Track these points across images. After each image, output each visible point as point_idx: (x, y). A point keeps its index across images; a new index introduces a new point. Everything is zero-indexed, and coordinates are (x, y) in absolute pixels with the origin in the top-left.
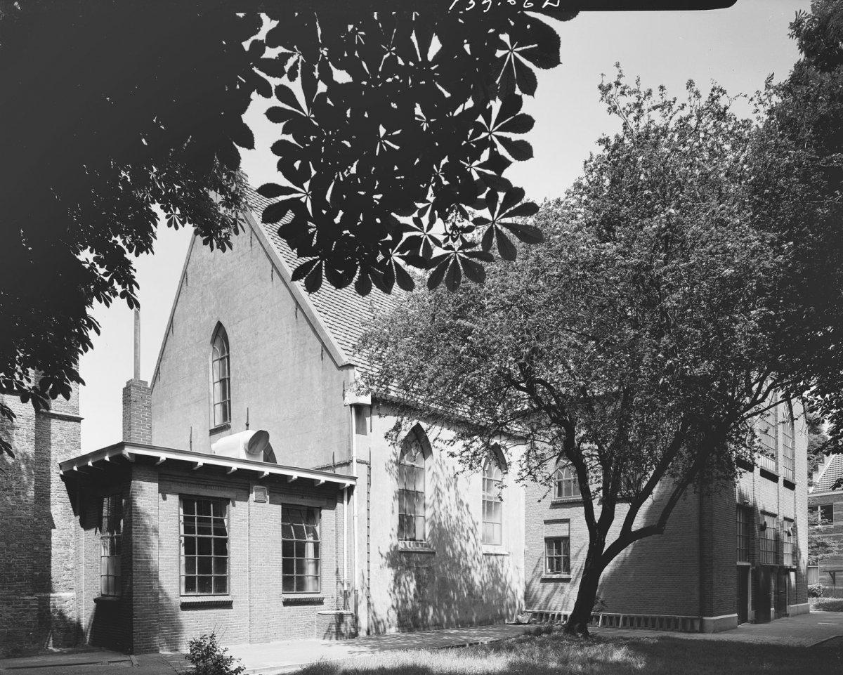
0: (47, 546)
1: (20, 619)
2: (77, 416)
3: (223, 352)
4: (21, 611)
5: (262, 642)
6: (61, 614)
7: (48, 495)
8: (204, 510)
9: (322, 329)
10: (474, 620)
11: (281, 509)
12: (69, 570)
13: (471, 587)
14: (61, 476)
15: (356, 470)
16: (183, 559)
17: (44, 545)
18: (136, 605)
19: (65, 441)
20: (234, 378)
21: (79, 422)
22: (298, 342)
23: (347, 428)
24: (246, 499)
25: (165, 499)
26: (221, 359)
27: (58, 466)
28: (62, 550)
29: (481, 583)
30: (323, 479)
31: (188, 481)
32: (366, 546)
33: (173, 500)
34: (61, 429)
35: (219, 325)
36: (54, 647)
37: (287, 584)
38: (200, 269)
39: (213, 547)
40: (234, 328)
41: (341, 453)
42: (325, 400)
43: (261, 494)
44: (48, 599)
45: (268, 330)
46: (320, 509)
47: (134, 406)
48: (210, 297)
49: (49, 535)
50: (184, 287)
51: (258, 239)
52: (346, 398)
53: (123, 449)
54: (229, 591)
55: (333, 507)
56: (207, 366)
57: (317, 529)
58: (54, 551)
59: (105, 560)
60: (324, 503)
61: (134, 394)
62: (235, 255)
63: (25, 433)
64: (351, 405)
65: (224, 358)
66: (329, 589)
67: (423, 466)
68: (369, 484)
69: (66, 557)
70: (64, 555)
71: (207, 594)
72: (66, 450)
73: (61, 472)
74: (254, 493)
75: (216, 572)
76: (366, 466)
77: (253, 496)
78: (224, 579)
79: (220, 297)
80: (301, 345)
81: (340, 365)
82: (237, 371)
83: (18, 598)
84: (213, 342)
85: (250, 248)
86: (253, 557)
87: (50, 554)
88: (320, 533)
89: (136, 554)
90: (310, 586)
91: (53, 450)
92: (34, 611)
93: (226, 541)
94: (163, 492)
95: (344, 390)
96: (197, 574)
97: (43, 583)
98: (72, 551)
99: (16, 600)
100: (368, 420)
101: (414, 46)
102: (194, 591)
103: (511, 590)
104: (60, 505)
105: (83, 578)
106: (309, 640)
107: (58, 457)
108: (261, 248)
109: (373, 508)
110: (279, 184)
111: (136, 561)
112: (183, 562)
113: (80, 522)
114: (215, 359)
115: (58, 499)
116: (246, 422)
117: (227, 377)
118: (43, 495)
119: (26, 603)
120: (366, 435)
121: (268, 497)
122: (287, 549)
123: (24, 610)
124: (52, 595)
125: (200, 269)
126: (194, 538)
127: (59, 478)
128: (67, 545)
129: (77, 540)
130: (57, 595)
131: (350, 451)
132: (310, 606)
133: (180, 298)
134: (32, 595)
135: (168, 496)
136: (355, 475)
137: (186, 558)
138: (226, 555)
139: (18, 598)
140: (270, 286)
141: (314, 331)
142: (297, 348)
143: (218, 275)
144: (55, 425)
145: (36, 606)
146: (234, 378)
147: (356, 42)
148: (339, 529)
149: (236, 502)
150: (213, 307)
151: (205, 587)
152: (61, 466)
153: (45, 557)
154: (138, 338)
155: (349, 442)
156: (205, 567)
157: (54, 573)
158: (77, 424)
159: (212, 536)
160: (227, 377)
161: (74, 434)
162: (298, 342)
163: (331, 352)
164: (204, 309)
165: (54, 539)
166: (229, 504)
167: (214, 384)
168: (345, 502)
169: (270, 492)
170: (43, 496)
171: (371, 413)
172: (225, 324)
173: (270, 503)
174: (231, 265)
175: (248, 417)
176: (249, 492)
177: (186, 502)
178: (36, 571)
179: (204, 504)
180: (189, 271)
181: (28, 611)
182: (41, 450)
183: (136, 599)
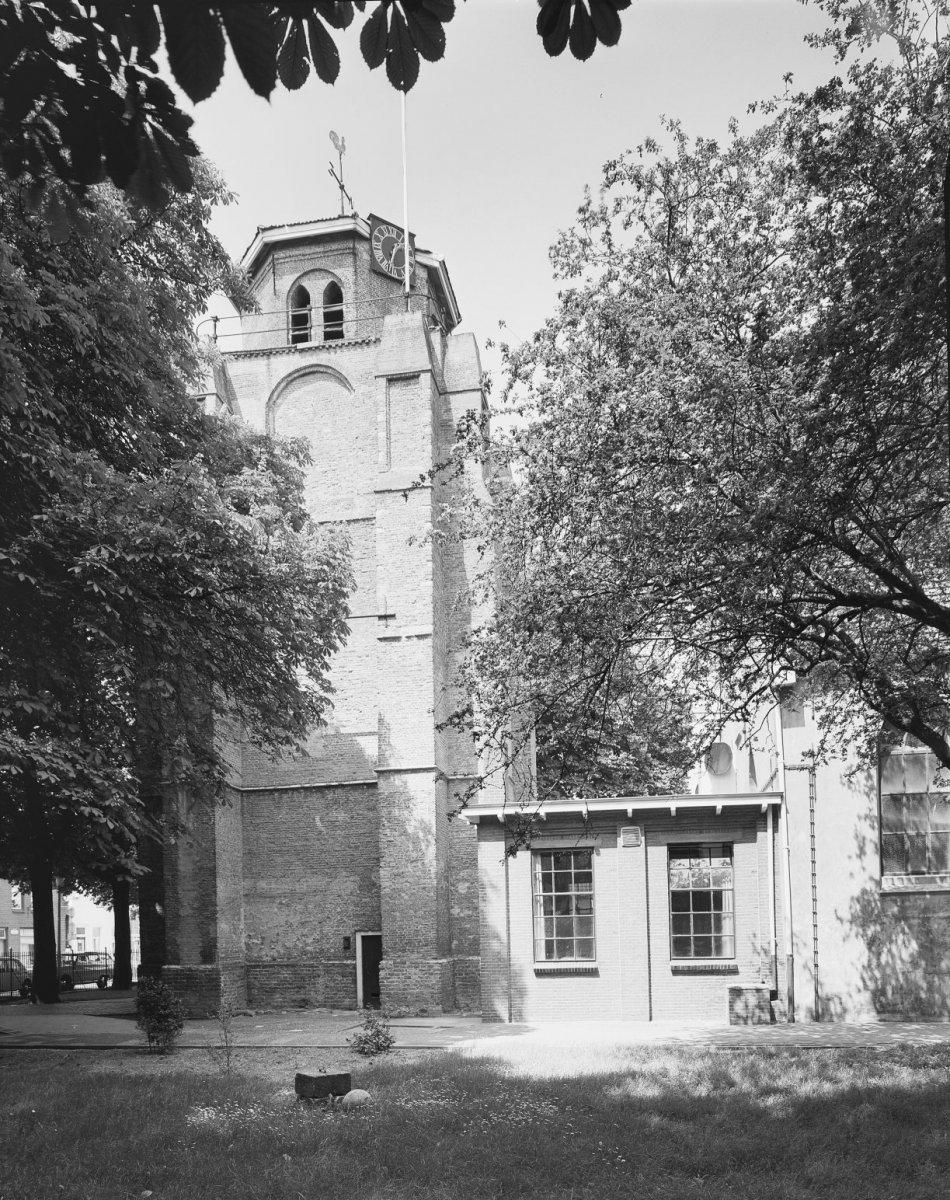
32: (810, 890)
43: (631, 838)
60: (738, 835)
75: (579, 934)
77: (621, 841)
90: (727, 951)
101: (328, 20)
102: (572, 955)
119: (431, 967)
147: (40, 19)
156: (565, 929)
158: (371, 791)
177: (542, 854)
179: (560, 857)
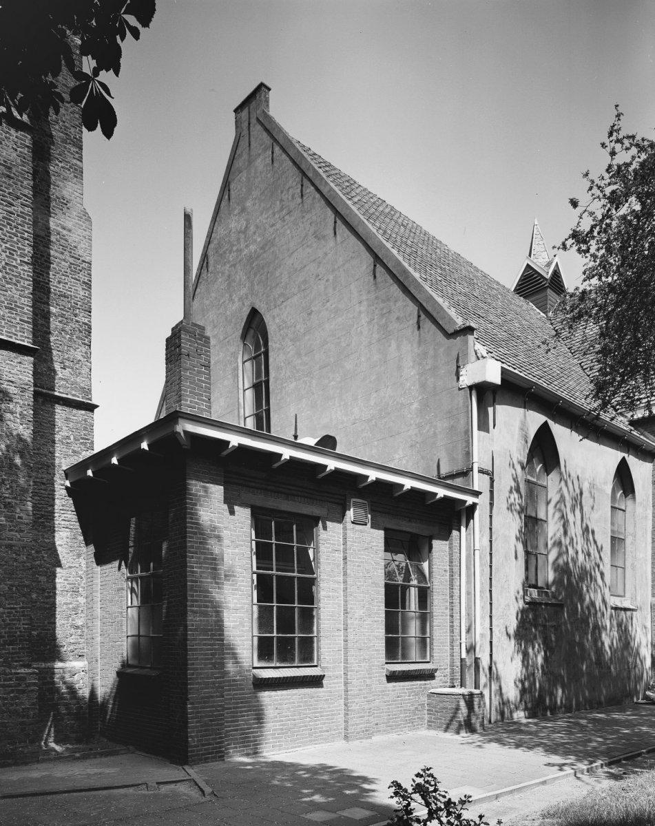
0: (49, 592)
1: (12, 705)
2: (90, 402)
3: (257, 348)
4: (12, 691)
5: (361, 738)
6: (72, 690)
7: (50, 516)
8: (284, 533)
9: (419, 286)
10: (603, 699)
11: (383, 536)
12: (77, 627)
13: (599, 651)
14: (67, 488)
15: (479, 482)
16: (255, 608)
17: (44, 590)
18: (191, 684)
19: (72, 437)
20: (276, 379)
21: (92, 411)
22: (377, 312)
23: (462, 422)
24: (340, 519)
25: (232, 512)
26: (254, 358)
27: (63, 475)
28: (68, 599)
29: (610, 648)
30: (441, 492)
31: (269, 487)
33: (243, 515)
34: (67, 419)
35: (254, 314)
36: (56, 742)
37: (394, 648)
38: (227, 246)
39: (296, 592)
40: (276, 311)
41: (452, 460)
42: (423, 386)
43: (361, 511)
44: (51, 672)
45: (328, 304)
46: (431, 538)
47: (186, 363)
48: (240, 280)
49: (54, 575)
50: (204, 275)
51: (313, 184)
52: (461, 378)
53: (177, 423)
54: (318, 659)
55: (446, 536)
56: (236, 369)
57: (425, 565)
58: (60, 599)
59: (133, 612)
61: (186, 345)
62: (277, 216)
63: (19, 410)
64: (471, 388)
65: (260, 355)
66: (441, 657)
67: (545, 484)
68: (492, 505)
69: (75, 609)
70: (71, 606)
71: (289, 665)
72: (74, 452)
73: (68, 483)
74: (352, 510)
76: (487, 478)
77: (350, 514)
78: (311, 640)
79: (255, 275)
80: (382, 315)
81: (451, 331)
82: (279, 368)
83: (8, 671)
84: (244, 337)
85: (299, 200)
86: (351, 609)
87: (53, 606)
88: (430, 573)
89: (193, 601)
91: (59, 448)
92: (33, 691)
93: (312, 582)
94: (231, 501)
95: (458, 367)
96: (275, 634)
97: (48, 649)
98: (82, 600)
99: (6, 674)
100: (490, 410)
103: (640, 658)
104: (67, 533)
105: (99, 639)
106: (419, 733)
107: (63, 460)
108: (318, 196)
109: (496, 539)
110: (128, 435)
111: (192, 611)
112: (256, 615)
113: (95, 556)
114: (245, 359)
115: (63, 522)
116: (293, 433)
117: (263, 379)
118: (42, 516)
119: (21, 679)
120: (488, 432)
121: (369, 516)
122: (394, 596)
123: (18, 691)
124: (59, 665)
125: (227, 246)
126: (271, 576)
127: (64, 492)
128: (75, 592)
129: (90, 585)
130: (68, 665)
131: (468, 454)
132: (419, 682)
133: (198, 290)
134: (29, 666)
135: (236, 508)
136: (476, 488)
137: (260, 607)
138: (313, 604)
139: (8, 671)
140: (331, 243)
141: (406, 290)
142: (375, 321)
143: (253, 248)
144: (60, 412)
145: (34, 684)
146: (276, 379)
148: (456, 569)
149: (328, 523)
150: (244, 291)
151: (286, 655)
152: (67, 474)
153: (46, 609)
154: (189, 267)
155: (467, 442)
156: (286, 624)
157: (60, 633)
159: (295, 574)
160: (263, 379)
161: (85, 429)
162: (377, 312)
163: (435, 314)
164: (231, 296)
165: (59, 581)
166: (317, 525)
167: (244, 391)
168: (463, 529)
169: (372, 511)
170: (44, 520)
171: (494, 401)
172: (262, 308)
173: (372, 527)
174: (271, 230)
175: (296, 426)
176: (344, 509)
178: (34, 630)
180: (210, 253)
181: (23, 692)
182: (39, 449)
183: (193, 674)
